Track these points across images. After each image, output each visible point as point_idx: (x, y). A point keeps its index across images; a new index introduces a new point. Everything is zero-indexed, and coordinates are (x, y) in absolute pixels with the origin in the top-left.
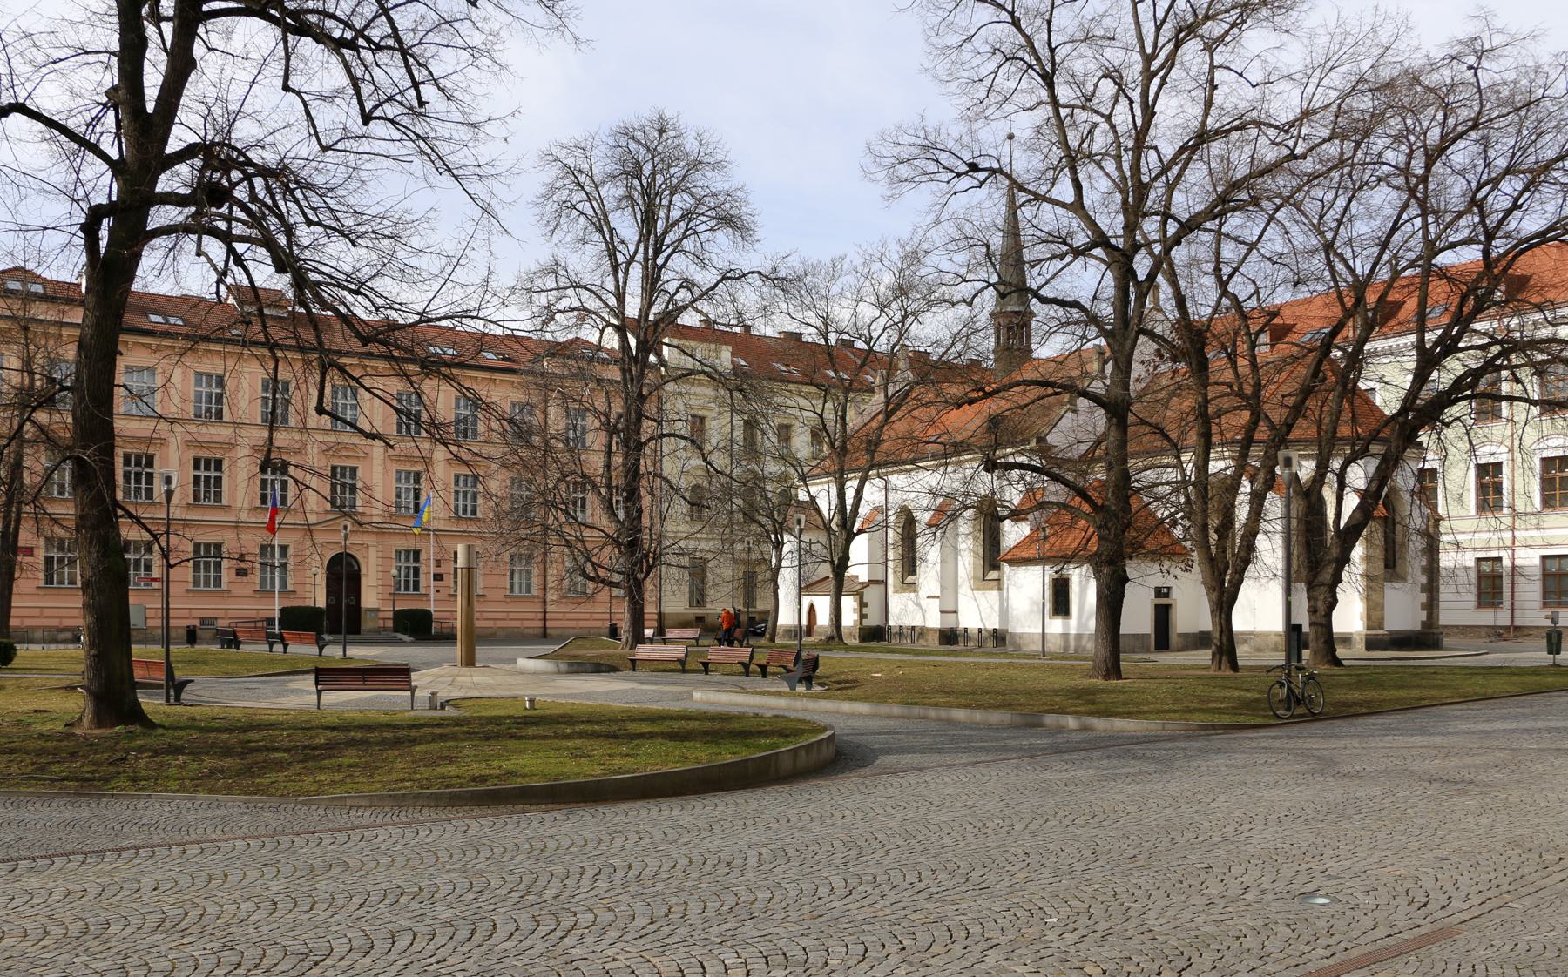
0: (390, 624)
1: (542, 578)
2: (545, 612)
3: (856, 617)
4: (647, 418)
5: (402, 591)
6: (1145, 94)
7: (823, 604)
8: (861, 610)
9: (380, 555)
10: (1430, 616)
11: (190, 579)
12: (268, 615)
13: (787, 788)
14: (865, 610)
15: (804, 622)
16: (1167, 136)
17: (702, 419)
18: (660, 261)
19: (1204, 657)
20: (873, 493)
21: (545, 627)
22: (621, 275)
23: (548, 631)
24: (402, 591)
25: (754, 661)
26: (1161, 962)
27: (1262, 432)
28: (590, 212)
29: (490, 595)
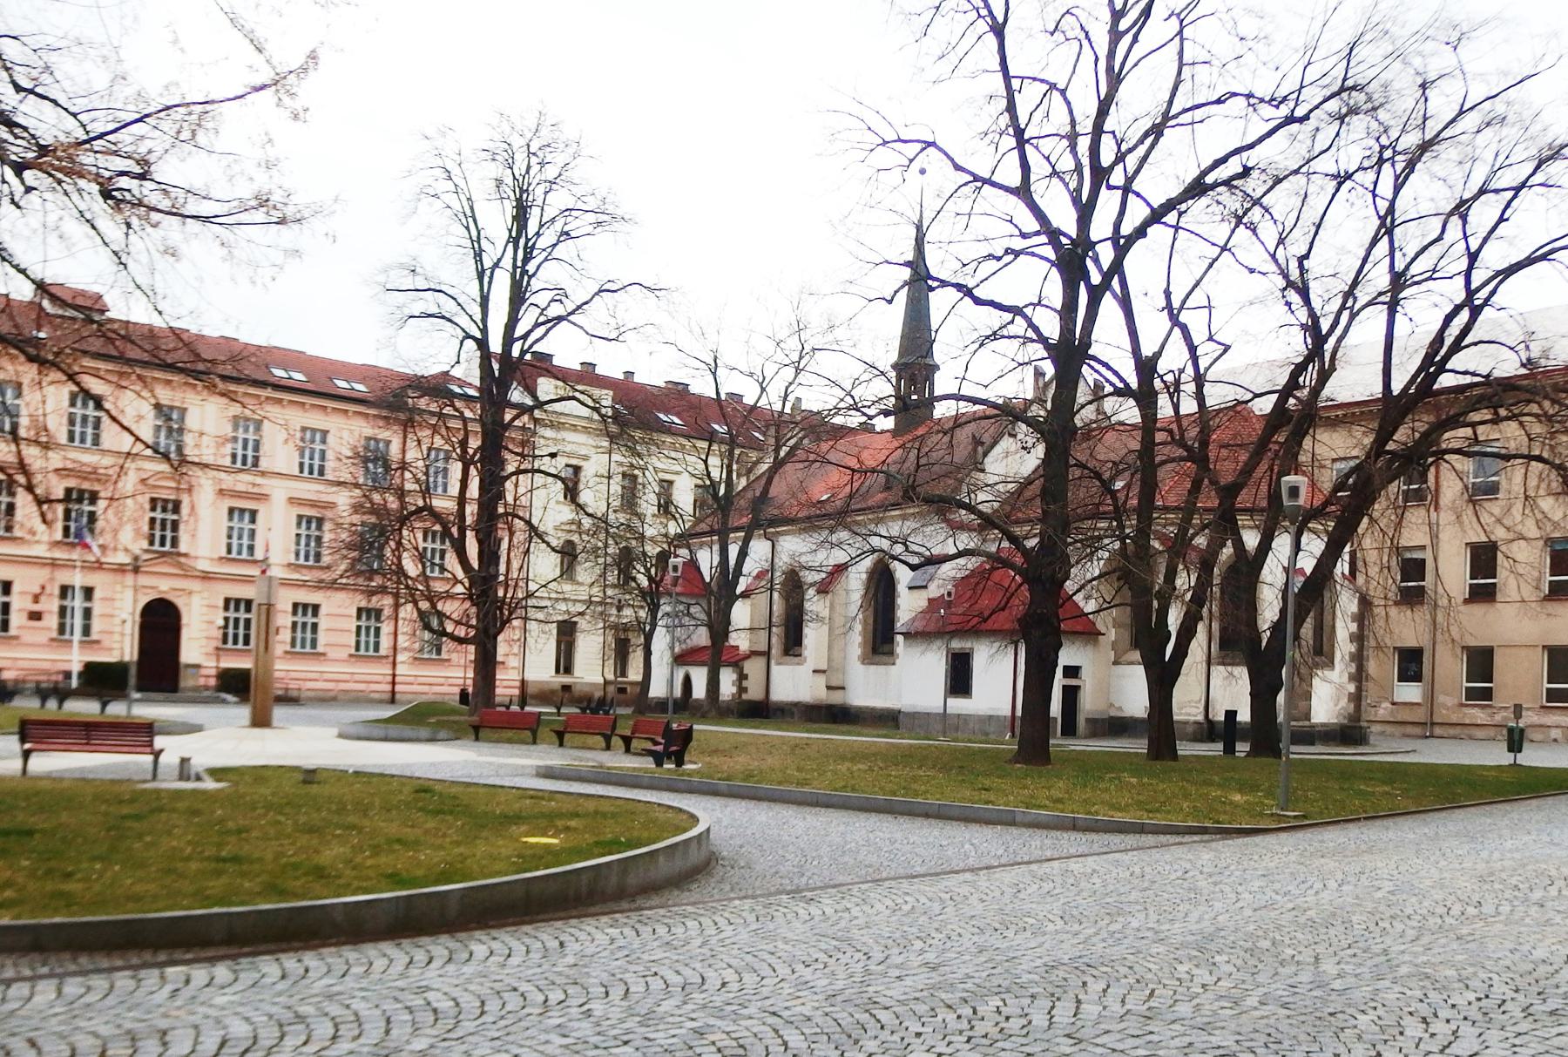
0: (213, 682)
1: (392, 637)
2: (394, 676)
3: (734, 690)
4: (1074, 594)
5: (362, 652)
6: (1111, 55)
7: (700, 677)
8: (740, 683)
9: (206, 602)
10: (1358, 708)
11: (353, 644)
12: (65, 667)
13: (941, 825)
14: (745, 683)
15: (678, 692)
16: (1131, 116)
17: (671, 483)
18: (531, 267)
19: (1139, 746)
20: (759, 549)
21: (393, 692)
22: (486, 279)
23: (398, 696)
24: (298, 649)
25: (618, 731)
26: (1154, 986)
27: (1209, 500)
28: (457, 206)
29: (332, 654)
